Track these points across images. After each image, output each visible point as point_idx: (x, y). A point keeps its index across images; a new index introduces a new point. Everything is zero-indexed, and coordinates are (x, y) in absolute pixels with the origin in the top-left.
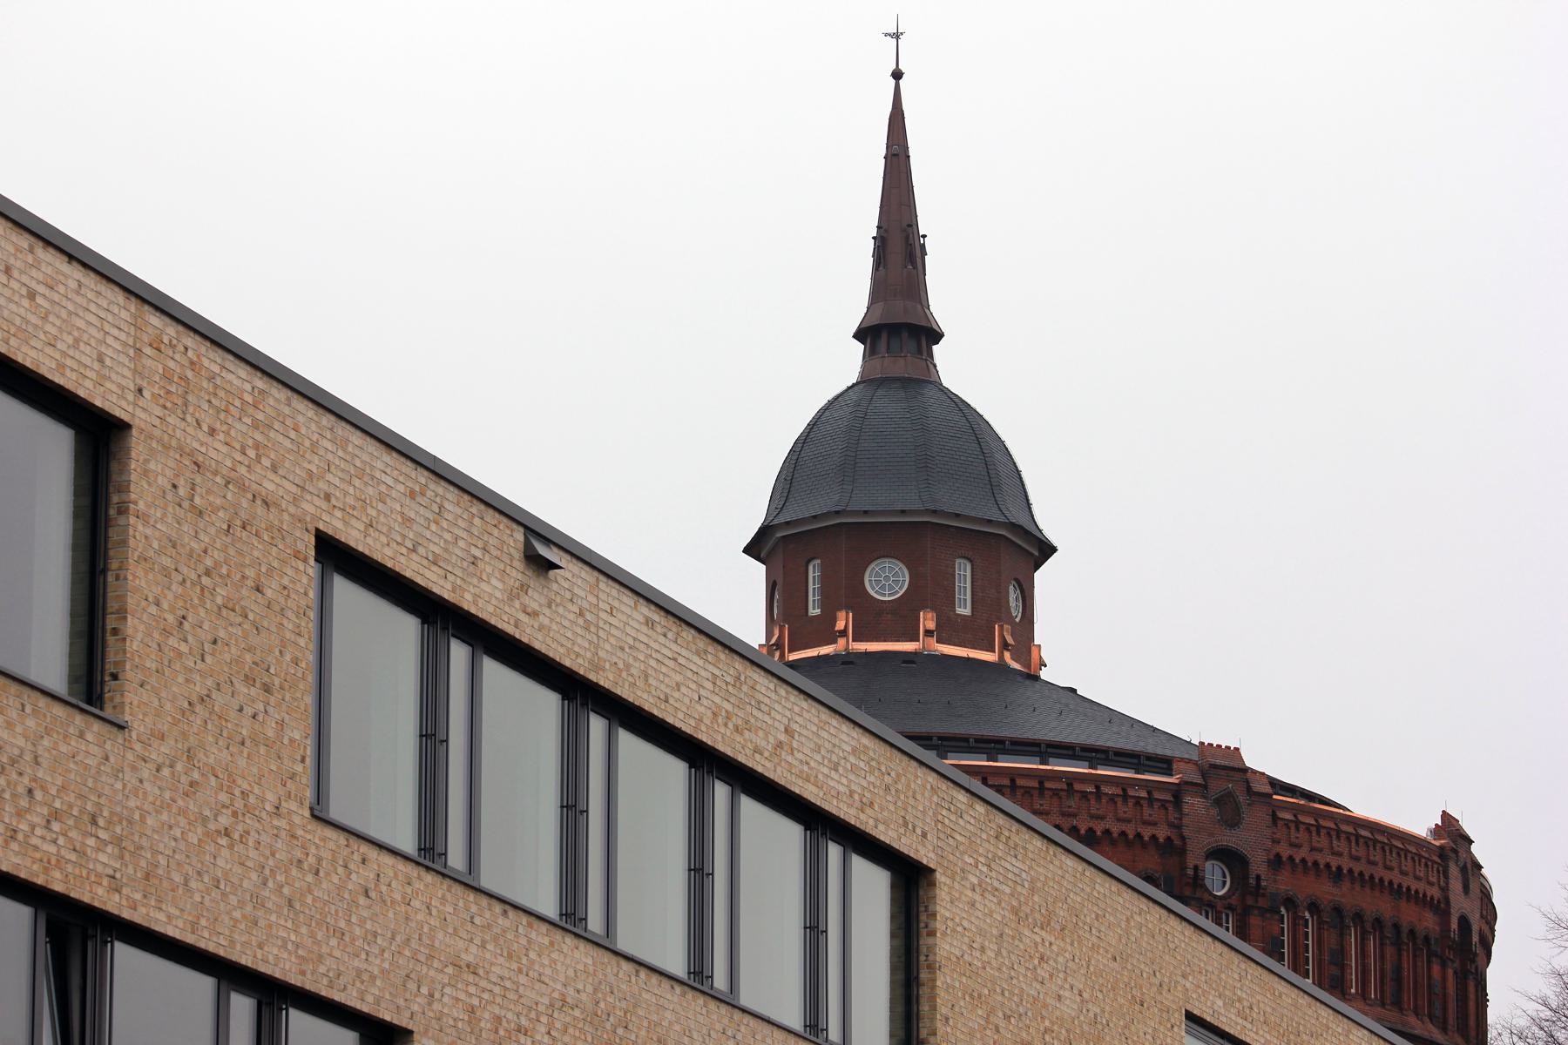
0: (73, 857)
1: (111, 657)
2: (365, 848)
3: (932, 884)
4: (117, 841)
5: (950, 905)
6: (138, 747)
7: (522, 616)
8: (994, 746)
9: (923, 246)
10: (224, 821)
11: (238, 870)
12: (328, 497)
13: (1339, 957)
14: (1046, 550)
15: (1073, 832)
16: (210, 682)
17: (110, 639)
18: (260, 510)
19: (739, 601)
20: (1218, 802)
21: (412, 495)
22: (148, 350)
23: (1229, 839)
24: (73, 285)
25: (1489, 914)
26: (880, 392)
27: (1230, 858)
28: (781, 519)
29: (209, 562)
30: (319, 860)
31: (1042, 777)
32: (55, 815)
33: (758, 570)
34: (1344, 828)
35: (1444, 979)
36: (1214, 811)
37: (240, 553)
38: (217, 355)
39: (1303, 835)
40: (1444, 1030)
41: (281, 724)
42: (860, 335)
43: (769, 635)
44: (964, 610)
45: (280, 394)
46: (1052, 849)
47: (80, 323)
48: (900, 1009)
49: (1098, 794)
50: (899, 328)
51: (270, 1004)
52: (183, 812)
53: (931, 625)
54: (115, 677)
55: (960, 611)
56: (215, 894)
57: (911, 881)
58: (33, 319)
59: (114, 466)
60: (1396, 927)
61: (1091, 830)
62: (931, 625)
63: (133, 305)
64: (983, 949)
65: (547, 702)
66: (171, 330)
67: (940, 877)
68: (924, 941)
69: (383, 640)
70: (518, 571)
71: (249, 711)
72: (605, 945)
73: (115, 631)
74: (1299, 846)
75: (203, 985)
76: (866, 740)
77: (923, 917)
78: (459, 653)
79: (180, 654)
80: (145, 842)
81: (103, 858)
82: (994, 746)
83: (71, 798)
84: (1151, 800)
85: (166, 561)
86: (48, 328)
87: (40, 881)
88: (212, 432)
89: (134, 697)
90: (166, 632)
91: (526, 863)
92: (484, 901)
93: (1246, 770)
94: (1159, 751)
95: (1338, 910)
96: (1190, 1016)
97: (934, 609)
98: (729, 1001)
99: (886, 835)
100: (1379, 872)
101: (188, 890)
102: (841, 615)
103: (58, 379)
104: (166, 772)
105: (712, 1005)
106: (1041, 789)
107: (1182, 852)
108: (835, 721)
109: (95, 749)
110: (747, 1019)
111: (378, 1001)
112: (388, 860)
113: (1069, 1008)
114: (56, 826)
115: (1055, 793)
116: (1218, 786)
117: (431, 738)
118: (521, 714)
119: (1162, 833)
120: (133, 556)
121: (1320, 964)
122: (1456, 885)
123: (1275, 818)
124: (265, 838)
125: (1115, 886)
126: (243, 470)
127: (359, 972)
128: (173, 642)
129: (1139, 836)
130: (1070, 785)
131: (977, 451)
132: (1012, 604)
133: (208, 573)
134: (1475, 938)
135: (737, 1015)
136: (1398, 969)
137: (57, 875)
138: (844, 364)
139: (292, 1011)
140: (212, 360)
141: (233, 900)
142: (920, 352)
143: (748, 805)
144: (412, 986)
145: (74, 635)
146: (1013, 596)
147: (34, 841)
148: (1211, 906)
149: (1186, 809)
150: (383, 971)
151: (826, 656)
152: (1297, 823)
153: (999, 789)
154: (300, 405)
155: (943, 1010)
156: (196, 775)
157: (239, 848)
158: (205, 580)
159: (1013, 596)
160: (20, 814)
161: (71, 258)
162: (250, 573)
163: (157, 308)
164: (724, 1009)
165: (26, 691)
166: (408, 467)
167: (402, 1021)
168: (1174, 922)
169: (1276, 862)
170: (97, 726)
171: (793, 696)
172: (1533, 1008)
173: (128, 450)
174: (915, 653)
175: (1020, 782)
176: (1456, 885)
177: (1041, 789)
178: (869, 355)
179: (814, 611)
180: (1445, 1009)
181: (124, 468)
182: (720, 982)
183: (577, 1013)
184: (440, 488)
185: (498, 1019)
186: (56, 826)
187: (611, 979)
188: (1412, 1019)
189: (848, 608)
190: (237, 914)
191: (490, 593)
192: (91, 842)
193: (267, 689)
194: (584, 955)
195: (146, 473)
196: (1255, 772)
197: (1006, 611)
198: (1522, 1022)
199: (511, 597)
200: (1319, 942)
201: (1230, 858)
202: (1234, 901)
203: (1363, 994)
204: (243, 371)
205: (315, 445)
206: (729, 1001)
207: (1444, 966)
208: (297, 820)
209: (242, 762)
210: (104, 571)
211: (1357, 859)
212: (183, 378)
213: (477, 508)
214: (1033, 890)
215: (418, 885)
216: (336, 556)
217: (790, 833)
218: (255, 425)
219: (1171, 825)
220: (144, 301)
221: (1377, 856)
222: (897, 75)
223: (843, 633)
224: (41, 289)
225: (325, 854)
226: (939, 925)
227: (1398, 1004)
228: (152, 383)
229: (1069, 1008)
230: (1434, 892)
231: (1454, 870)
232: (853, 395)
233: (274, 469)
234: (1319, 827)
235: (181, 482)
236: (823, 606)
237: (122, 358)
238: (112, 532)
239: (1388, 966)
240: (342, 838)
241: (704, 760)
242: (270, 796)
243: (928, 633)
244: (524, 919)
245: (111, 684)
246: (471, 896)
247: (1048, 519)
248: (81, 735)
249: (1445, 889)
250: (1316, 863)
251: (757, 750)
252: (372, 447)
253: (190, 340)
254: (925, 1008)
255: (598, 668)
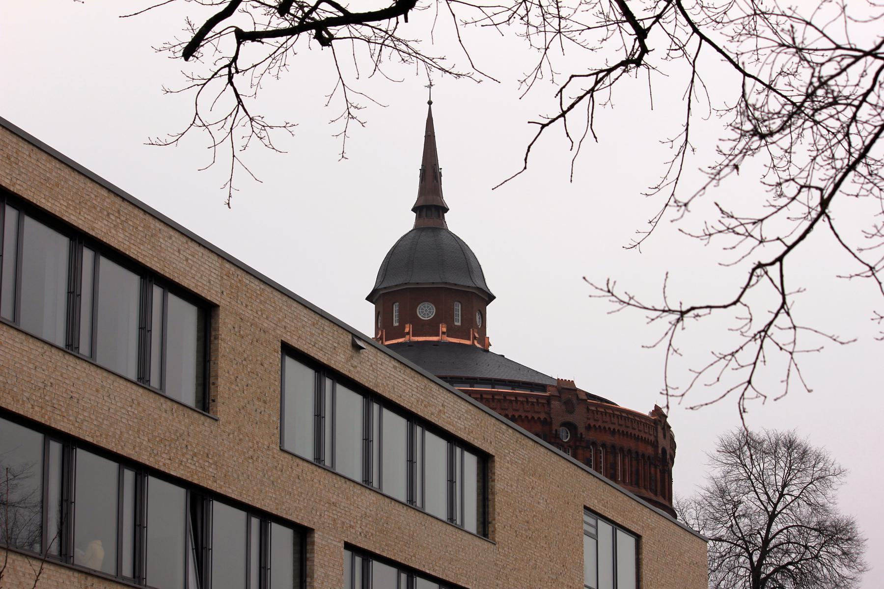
0: (201, 470)
1: (212, 393)
2: (298, 460)
3: (494, 461)
4: (215, 463)
5: (501, 471)
6: (222, 427)
7: (351, 368)
8: (473, 381)
9: (440, 173)
10: (251, 453)
11: (255, 471)
12: (285, 327)
13: (614, 466)
14: (491, 298)
15: (506, 416)
16: (246, 401)
17: (212, 386)
18: (263, 334)
19: (363, 319)
20: (566, 403)
21: (314, 324)
22: (225, 277)
23: (570, 418)
24: (200, 254)
25: (673, 446)
26: (423, 234)
27: (571, 426)
28: (382, 286)
29: (245, 356)
30: (283, 466)
31: (493, 394)
32: (195, 455)
33: (372, 307)
34: (616, 413)
35: (656, 473)
36: (564, 407)
37: (256, 351)
38: (248, 277)
39: (599, 416)
40: (656, 495)
41: (270, 415)
43: (376, 334)
44: (458, 324)
45: (269, 289)
46: (536, 445)
47: (203, 269)
48: (481, 510)
49: (516, 401)
50: (430, 207)
51: (141, 474)
52: (237, 451)
53: (444, 330)
54: (214, 401)
55: (456, 324)
56: (248, 481)
57: (485, 460)
58: (188, 269)
59: (213, 321)
60: (637, 452)
61: (513, 416)
62: (444, 330)
63: (220, 260)
64: (512, 486)
65: (134, 280)
66: (233, 269)
67: (496, 459)
68: (490, 483)
69: (301, 378)
70: (349, 351)
71: (259, 411)
72: (379, 492)
73: (214, 384)
74: (598, 421)
75: (242, 515)
76: (470, 407)
77: (490, 474)
78: (88, 255)
79: (236, 391)
80: (224, 463)
81: (210, 470)
82: (473, 381)
83: (200, 448)
84: (538, 403)
85: (231, 356)
86: (192, 271)
87: (190, 480)
88: (246, 306)
89: (223, 408)
90: (231, 383)
91: (350, 462)
92: (339, 478)
93: (576, 390)
94: (540, 382)
95: (613, 447)
96: (586, 508)
97: (445, 323)
98: (421, 511)
99: (477, 443)
100: (630, 431)
101: (239, 480)
102: (407, 326)
103: (196, 291)
104: (231, 436)
105: (417, 513)
106: (493, 399)
107: (551, 424)
108: (459, 401)
109: (208, 429)
110: (429, 518)
111: (50, 418)
112: (306, 464)
113: (542, 506)
114: (195, 459)
115: (499, 400)
117: (144, 329)
118: (349, 404)
119: (542, 416)
120: (220, 355)
121: (606, 470)
122: (660, 435)
123: (588, 409)
124: (265, 459)
125: (558, 458)
126: (257, 320)
127: (296, 507)
128: (233, 386)
129: (533, 418)
130: (505, 397)
131: (463, 259)
132: (478, 320)
133: (245, 360)
134: (668, 457)
135: (426, 516)
136: (638, 470)
137: (196, 477)
138: (408, 222)
139: (78, 450)
140: (247, 279)
141: (254, 483)
142: (439, 216)
143: (340, 388)
144: (314, 512)
145: (197, 385)
146: (478, 317)
147: (188, 465)
148: (563, 446)
149: (552, 406)
150: (304, 507)
151: (401, 343)
152: (597, 411)
153: (476, 399)
154: (276, 293)
155: (498, 510)
156: (241, 436)
157: (256, 463)
158: (244, 362)
159: (478, 317)
160: (183, 455)
161: (200, 244)
162: (259, 358)
163: (228, 261)
164: (421, 514)
165: (185, 409)
166: (312, 314)
167: (310, 525)
168: (579, 471)
169: (588, 428)
170: (208, 420)
171: (445, 392)
172: (703, 492)
173: (218, 316)
174: (438, 342)
175: (484, 396)
176: (660, 435)
177: (493, 399)
178: (418, 218)
179: (396, 324)
180: (656, 486)
181: (217, 322)
182: (328, 463)
183: (370, 519)
184: (323, 321)
185: (343, 523)
186: (195, 459)
187: (382, 505)
188: (643, 491)
189: (410, 323)
190: (255, 488)
191: (340, 361)
192: (207, 464)
193: (265, 402)
194: (372, 497)
195: (224, 323)
196: (580, 390)
197: (475, 324)
198: (700, 498)
199: (348, 360)
200: (606, 460)
201: (571, 426)
202: (571, 444)
203: (624, 481)
204: (257, 282)
205: (281, 308)
206: (421, 511)
207: (656, 468)
208: (275, 451)
209: (257, 430)
210: (209, 361)
211: (621, 425)
212: (237, 286)
213: (335, 328)
214: (529, 462)
215: (316, 473)
216: (288, 350)
217: (309, 374)
218: (261, 302)
219: (546, 413)
220: (224, 258)
221: (635, 425)
222: (430, 103)
223: (408, 333)
224: (190, 257)
225: (285, 464)
226: (496, 478)
227: (637, 484)
228: (226, 289)
229: (542, 506)
230: (652, 438)
231: (659, 428)
232: (412, 235)
233: (267, 318)
234: (606, 413)
235: (236, 326)
236: (399, 322)
237: (217, 281)
238: (212, 346)
239: (634, 469)
240: (290, 457)
241: (412, 418)
242: (266, 443)
243: (443, 333)
244: (352, 484)
245: (212, 404)
246: (334, 477)
247: (492, 285)
248: (203, 424)
249: (656, 437)
250: (605, 428)
251: (432, 414)
252: (300, 308)
253: (239, 272)
254: (491, 510)
255: (377, 386)
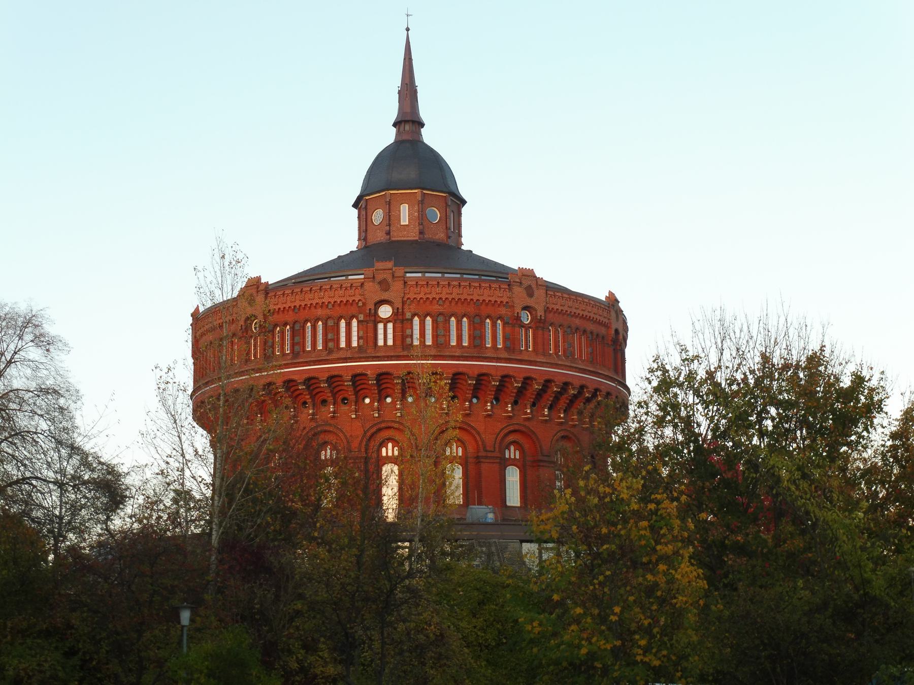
14: (464, 202)
20: (380, 283)
23: (530, 302)
42: (395, 125)
50: (409, 121)
116: (526, 283)
138: (389, 136)
178: (398, 133)
222: (408, 29)
230: (606, 320)
